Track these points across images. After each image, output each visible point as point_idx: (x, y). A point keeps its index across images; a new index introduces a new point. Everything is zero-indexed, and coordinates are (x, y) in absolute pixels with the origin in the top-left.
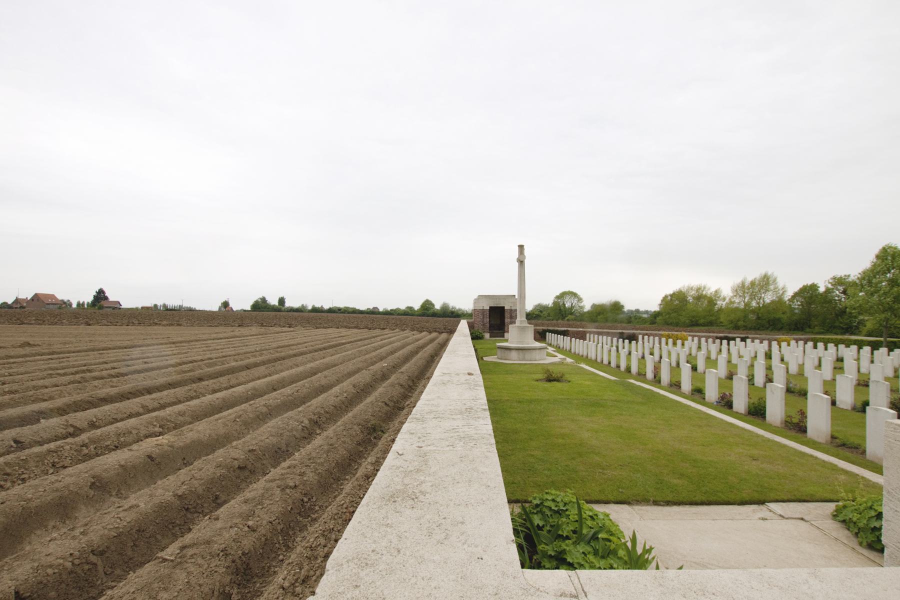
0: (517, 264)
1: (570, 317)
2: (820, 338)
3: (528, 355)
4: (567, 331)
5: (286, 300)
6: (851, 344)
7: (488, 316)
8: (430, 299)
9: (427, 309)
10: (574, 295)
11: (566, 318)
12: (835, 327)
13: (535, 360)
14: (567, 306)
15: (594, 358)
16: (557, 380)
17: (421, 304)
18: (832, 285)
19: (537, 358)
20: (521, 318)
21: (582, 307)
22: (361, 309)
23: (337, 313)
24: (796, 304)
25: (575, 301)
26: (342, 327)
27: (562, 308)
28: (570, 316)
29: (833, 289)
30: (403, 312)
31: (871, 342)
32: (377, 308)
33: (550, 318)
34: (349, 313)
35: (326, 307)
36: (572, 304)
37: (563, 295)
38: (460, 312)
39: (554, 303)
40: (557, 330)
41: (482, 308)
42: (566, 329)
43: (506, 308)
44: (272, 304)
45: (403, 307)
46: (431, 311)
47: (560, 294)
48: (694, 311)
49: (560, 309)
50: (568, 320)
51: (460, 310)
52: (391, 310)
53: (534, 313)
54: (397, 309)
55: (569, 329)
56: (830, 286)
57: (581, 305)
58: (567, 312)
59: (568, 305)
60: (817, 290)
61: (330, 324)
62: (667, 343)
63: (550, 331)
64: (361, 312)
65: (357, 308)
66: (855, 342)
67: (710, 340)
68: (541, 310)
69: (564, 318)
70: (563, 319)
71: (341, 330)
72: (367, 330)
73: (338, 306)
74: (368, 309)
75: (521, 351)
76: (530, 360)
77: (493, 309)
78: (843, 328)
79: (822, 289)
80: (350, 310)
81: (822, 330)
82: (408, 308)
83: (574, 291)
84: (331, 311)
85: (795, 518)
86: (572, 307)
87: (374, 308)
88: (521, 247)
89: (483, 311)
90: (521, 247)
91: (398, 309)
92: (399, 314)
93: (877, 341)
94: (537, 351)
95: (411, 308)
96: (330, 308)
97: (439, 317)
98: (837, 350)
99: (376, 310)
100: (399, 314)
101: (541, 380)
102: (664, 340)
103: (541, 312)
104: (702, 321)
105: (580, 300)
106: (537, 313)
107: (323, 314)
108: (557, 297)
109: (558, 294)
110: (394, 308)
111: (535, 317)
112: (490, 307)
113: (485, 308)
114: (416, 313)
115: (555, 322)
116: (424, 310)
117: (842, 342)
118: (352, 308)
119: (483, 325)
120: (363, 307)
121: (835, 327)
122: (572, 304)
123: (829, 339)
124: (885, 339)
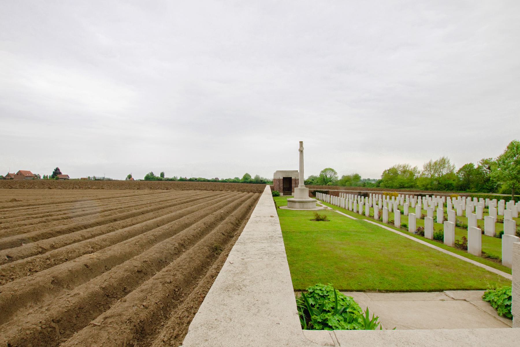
0: (298, 153)
2: (475, 195)
3: (305, 205)
4: (328, 191)
6: (493, 198)
7: (282, 183)
8: (248, 173)
10: (332, 170)
11: (328, 184)
12: (484, 189)
13: (310, 208)
14: (328, 177)
15: (344, 207)
17: (243, 176)
18: (482, 164)
19: (311, 207)
21: (336, 178)
26: (197, 189)
28: (330, 183)
29: (482, 166)
31: (504, 197)
32: (217, 178)
34: (201, 181)
35: (188, 178)
36: (331, 176)
37: (326, 170)
38: (266, 181)
39: (320, 175)
41: (278, 178)
42: (327, 190)
43: (292, 178)
45: (233, 178)
46: (249, 180)
47: (324, 170)
48: (402, 179)
49: (324, 179)
51: (266, 179)
54: (229, 179)
55: (329, 190)
56: (480, 165)
57: (336, 176)
58: (328, 181)
60: (473, 167)
62: (386, 198)
64: (208, 181)
66: (495, 197)
67: (411, 196)
70: (326, 184)
77: (285, 179)
78: (488, 189)
79: (476, 167)
81: (476, 190)
82: (236, 178)
83: (332, 168)
84: (190, 180)
85: (461, 300)
87: (216, 178)
88: (301, 143)
89: (279, 180)
90: (301, 143)
92: (230, 182)
93: (508, 196)
94: (311, 203)
98: (485, 202)
99: (217, 180)
102: (384, 196)
103: (313, 180)
104: (406, 185)
105: (335, 173)
106: (311, 181)
107: (186, 182)
108: (322, 172)
109: (323, 170)
113: (280, 178)
114: (241, 181)
116: (245, 179)
117: (488, 197)
118: (203, 179)
119: (280, 188)
120: (210, 178)
121: (484, 189)
122: (331, 176)
123: (480, 195)
124: (513, 196)
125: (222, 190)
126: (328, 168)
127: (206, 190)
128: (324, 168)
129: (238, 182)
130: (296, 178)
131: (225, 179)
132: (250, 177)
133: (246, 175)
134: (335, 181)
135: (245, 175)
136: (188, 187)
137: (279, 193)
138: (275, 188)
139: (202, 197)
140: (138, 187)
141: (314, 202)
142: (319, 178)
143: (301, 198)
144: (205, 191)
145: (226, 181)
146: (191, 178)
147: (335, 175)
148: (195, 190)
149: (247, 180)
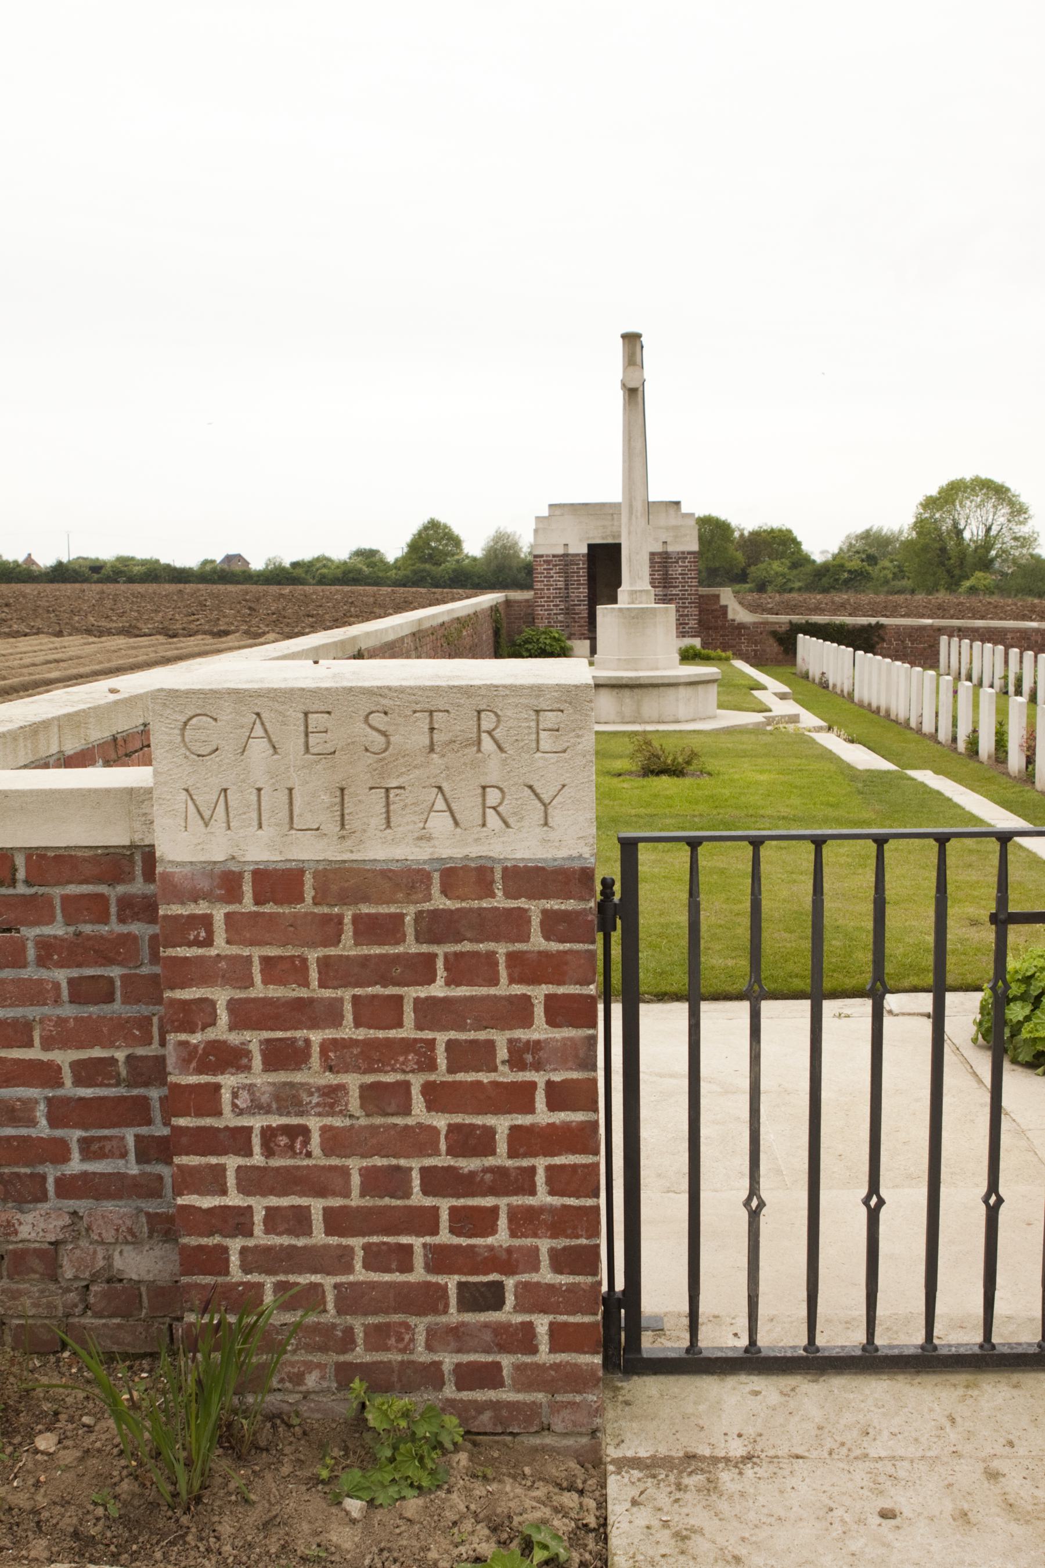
1: (979, 578)
3: (652, 704)
4: (879, 626)
5: (928, 495)
7: (583, 580)
8: (443, 519)
9: (435, 558)
10: (998, 492)
11: (967, 584)
13: (677, 722)
14: (967, 535)
15: (902, 718)
16: (676, 771)
17: (408, 538)
19: (682, 712)
20: (631, 584)
22: (179, 563)
23: (86, 580)
24: (914, 535)
25: (1000, 517)
26: (75, 631)
27: (951, 544)
28: (979, 574)
30: (339, 573)
32: (239, 557)
33: (905, 583)
34: (131, 580)
35: (45, 560)
36: (988, 530)
39: (920, 525)
40: (842, 627)
41: (560, 551)
42: (873, 621)
44: (406, 550)
45: (340, 552)
46: (450, 564)
49: (943, 550)
50: (973, 590)
52: (295, 565)
53: (842, 566)
54: (318, 559)
55: (884, 621)
57: (1024, 530)
58: (970, 560)
59: (973, 531)
61: (38, 623)
63: (951, 632)
64: (179, 576)
65: (164, 560)
68: (872, 551)
69: (958, 584)
70: (953, 585)
71: (66, 640)
72: (161, 639)
73: (92, 555)
74: (206, 562)
75: (627, 692)
76: (660, 722)
80: (136, 569)
82: (359, 553)
83: (998, 479)
84: (61, 573)
85: (914, 1014)
86: (987, 544)
87: (229, 558)
88: (632, 340)
89: (566, 560)
90: (632, 340)
91: (323, 561)
92: (322, 581)
94: (682, 691)
95: (369, 556)
96: (60, 564)
97: (256, 583)
99: (237, 567)
100: (322, 581)
101: (630, 773)
103: (872, 559)
105: (1018, 511)
106: (855, 564)
107: (29, 588)
108: (930, 503)
109: (934, 492)
110: (306, 555)
111: (846, 582)
112: (590, 547)
113: (572, 551)
114: (392, 573)
115: (920, 597)
116: (423, 560)
118: (144, 563)
119: (568, 611)
120: (188, 559)
122: (988, 530)
125: (226, 633)
126: (968, 476)
127: (128, 632)
128: (944, 482)
129: (377, 582)
130: (670, 549)
131: (287, 563)
132: (457, 542)
133: (426, 528)
134: (1015, 562)
135: (420, 533)
136: (22, 620)
137: (569, 643)
138: (539, 611)
139: (75, 671)
140: (616, 1441)
141: (700, 688)
142: (908, 544)
143: (631, 663)
144: (121, 641)
145: (299, 572)
146: (65, 560)
147: (1012, 525)
148: (59, 634)
149: (438, 564)
